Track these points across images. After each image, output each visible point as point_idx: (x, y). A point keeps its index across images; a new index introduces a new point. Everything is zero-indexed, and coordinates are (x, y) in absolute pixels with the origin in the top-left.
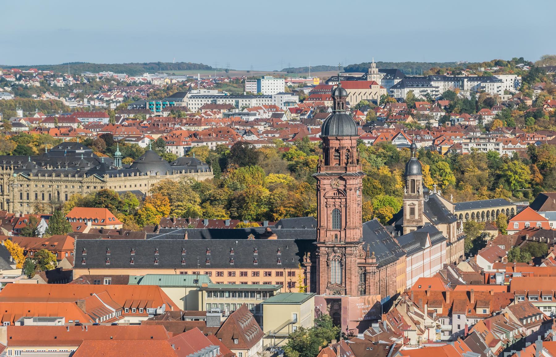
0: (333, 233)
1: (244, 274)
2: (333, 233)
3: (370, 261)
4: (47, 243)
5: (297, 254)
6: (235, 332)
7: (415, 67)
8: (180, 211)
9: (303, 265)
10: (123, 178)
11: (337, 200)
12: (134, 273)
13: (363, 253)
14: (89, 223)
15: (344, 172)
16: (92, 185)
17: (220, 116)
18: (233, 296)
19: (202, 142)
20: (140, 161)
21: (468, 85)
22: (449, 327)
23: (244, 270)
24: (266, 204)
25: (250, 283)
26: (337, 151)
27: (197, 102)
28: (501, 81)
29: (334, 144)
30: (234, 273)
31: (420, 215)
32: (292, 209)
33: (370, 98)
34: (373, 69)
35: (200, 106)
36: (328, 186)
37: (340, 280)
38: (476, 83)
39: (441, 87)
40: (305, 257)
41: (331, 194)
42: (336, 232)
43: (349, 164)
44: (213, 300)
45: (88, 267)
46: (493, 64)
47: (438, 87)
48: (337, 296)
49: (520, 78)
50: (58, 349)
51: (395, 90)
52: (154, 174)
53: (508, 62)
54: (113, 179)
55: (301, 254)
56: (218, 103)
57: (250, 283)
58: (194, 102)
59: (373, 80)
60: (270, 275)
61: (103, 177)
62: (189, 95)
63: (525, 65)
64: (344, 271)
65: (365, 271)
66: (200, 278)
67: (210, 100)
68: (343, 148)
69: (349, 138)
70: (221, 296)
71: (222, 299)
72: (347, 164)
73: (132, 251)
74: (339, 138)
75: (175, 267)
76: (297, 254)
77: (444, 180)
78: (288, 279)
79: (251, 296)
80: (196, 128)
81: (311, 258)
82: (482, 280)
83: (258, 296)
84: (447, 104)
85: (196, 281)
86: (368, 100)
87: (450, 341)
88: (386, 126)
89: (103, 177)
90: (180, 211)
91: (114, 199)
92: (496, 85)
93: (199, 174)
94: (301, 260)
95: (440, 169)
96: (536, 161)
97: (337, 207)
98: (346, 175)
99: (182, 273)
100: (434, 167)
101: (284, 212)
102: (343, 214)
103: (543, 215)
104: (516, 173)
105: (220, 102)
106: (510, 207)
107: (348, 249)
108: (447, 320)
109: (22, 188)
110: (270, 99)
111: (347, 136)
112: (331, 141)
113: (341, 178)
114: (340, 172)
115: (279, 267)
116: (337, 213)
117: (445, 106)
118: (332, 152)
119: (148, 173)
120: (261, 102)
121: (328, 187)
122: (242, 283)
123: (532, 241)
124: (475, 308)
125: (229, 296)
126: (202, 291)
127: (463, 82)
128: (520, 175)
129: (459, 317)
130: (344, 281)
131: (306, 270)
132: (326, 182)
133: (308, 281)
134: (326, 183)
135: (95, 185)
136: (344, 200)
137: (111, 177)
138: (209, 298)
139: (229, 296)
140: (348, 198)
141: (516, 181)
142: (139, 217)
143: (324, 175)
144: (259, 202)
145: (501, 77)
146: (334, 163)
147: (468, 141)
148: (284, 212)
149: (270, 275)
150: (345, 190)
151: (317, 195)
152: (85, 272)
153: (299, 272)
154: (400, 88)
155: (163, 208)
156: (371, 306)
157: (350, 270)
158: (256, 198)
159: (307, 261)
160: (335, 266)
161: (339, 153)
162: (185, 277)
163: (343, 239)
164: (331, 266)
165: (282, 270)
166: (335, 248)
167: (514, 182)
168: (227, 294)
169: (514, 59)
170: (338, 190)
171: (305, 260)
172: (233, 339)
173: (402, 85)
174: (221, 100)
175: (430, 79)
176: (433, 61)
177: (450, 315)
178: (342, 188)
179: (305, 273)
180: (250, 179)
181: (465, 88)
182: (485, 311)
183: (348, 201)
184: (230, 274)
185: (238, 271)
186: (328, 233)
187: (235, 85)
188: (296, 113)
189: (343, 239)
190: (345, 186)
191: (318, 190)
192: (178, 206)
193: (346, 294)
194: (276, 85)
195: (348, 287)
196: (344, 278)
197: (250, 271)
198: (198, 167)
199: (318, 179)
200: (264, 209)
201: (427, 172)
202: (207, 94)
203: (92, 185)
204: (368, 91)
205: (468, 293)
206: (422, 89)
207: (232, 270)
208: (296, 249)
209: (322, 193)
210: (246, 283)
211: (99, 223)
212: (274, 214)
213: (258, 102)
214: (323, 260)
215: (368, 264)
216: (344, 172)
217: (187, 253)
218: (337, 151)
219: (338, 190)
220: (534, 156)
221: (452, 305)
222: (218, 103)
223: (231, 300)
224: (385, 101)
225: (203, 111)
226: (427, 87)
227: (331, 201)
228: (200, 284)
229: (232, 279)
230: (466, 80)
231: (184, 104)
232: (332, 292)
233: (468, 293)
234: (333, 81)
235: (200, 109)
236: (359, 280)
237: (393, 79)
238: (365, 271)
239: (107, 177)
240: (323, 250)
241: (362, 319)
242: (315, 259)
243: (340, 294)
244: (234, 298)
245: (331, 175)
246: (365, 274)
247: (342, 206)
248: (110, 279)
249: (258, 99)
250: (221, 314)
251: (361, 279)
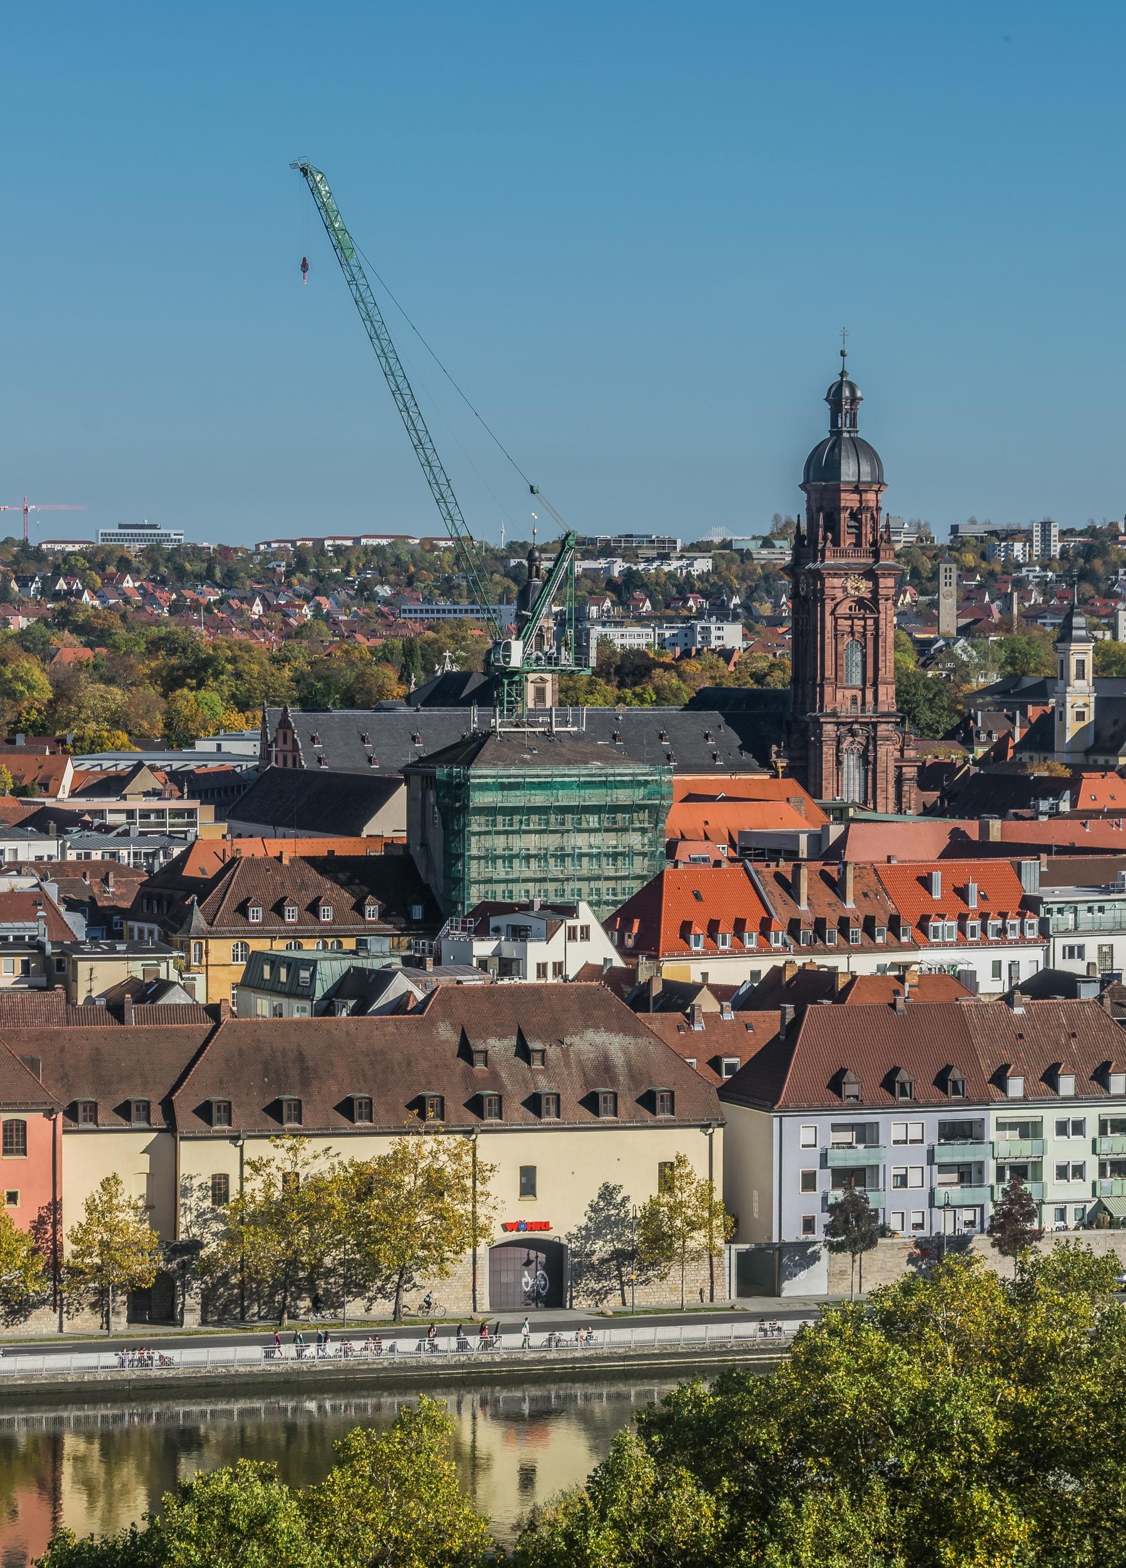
41: (843, 610)
42: (854, 692)
132: (837, 582)
136: (870, 622)
161: (860, 521)
183: (882, 623)
227: (844, 624)
240: (829, 730)
247: (869, 634)
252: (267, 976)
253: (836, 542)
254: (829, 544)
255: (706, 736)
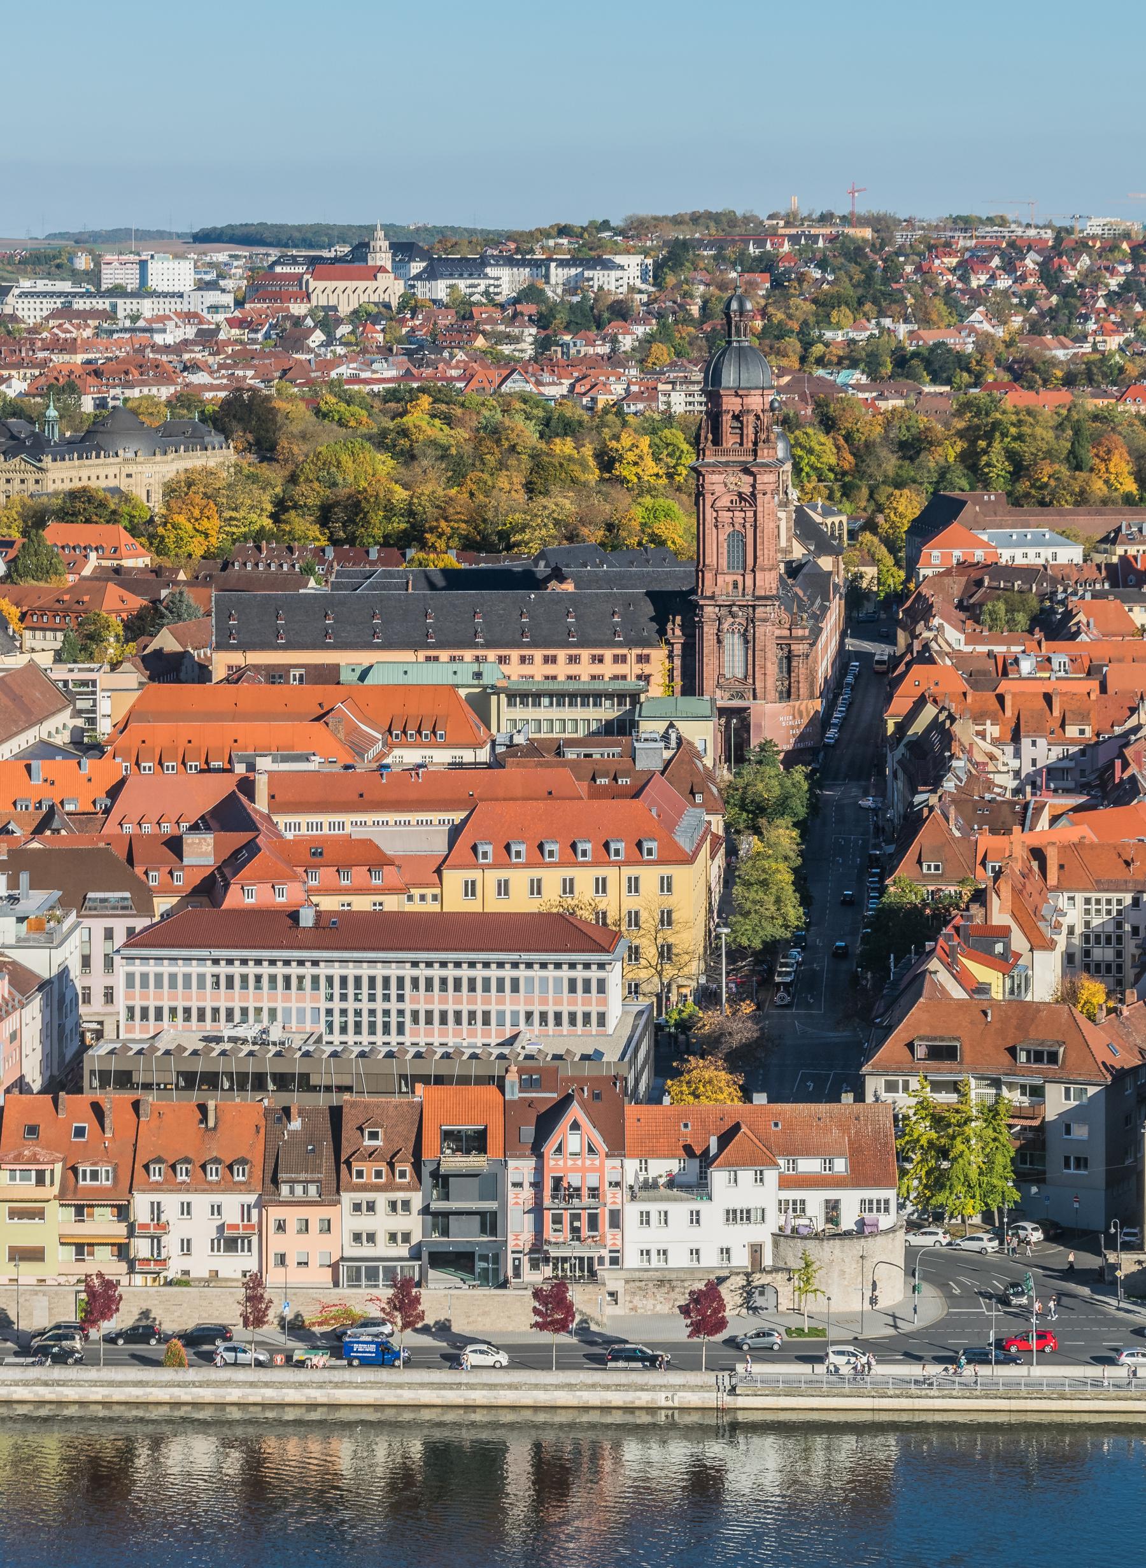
0: (730, 579)
1: (550, 660)
2: (730, 579)
3: (800, 633)
4: (66, 597)
5: (652, 619)
6: (695, 781)
7: (336, 233)
8: (234, 530)
9: (668, 642)
10: (77, 462)
11: (737, 514)
12: (348, 660)
13: (786, 617)
14: (93, 555)
15: (751, 459)
16: (17, 477)
17: (88, 333)
18: (558, 705)
19: (132, 387)
20: (101, 429)
21: (558, 275)
22: (1015, 764)
23: (550, 652)
24: (402, 515)
25: (561, 678)
26: (736, 417)
27: (32, 306)
28: (622, 268)
29: (731, 404)
30: (532, 658)
31: (789, 540)
32: (464, 526)
33: (375, 298)
34: (379, 243)
35: (45, 313)
36: (722, 485)
37: (743, 670)
38: (573, 271)
39: (507, 281)
40: (670, 626)
41: (724, 502)
42: (735, 577)
43: (761, 444)
44: (520, 712)
45: (244, 647)
46: (554, 232)
47: (498, 279)
48: (737, 703)
49: (649, 261)
50: (413, 817)
51: (419, 284)
52: (130, 455)
53: (584, 229)
54: (59, 464)
55: (661, 621)
56: (75, 306)
57: (585, 678)
58: (26, 306)
59: (379, 263)
60: (601, 661)
61: (40, 461)
62: (16, 291)
63: (616, 234)
64: (750, 652)
65: (790, 651)
66: (485, 668)
67: (58, 301)
68: (748, 411)
69: (760, 392)
70: (534, 705)
71: (537, 709)
72: (755, 444)
73: (326, 615)
74: (740, 392)
75: (415, 646)
76: (652, 619)
77: (677, 465)
78: (637, 669)
79: (595, 705)
80: (67, 357)
81: (683, 627)
82: (992, 668)
83: (608, 703)
84: (534, 312)
85: (478, 675)
86: (376, 304)
87: (489, 766)
88: (446, 354)
89: (40, 461)
90: (234, 530)
91: (102, 505)
92: (614, 274)
93: (209, 452)
94: (662, 632)
95: (668, 445)
96: (832, 427)
97: (737, 527)
98: (758, 465)
99: (428, 659)
100: (657, 441)
101: (448, 531)
102: (750, 541)
103: (985, 538)
104: (810, 451)
105: (80, 304)
106: (836, 520)
107: (759, 610)
108: (1009, 750)
109: (9, 487)
110: (179, 300)
111: (756, 388)
112: (725, 399)
113: (747, 471)
114: (742, 459)
115: (620, 645)
116: (737, 540)
117: (530, 316)
118: (727, 419)
119: (121, 452)
120: (167, 306)
121: (719, 489)
122: (547, 678)
123: (998, 588)
124: (1063, 726)
125: (551, 704)
126: (498, 694)
127: (548, 269)
128: (819, 457)
129: (1034, 743)
130: (750, 672)
131: (671, 651)
132: (715, 478)
133: (677, 673)
134: (714, 480)
135: (22, 476)
136: (750, 514)
137: (55, 460)
138: (512, 709)
139: (551, 704)
140: (760, 509)
141: (812, 467)
142: (161, 542)
143: (714, 465)
144: (390, 510)
145: (619, 259)
146: (730, 441)
147: (669, 387)
148: (448, 531)
149: (601, 661)
150: (753, 494)
151: (697, 504)
152: (237, 658)
153: (659, 655)
154: (428, 279)
155: (205, 524)
156: (805, 721)
157: (763, 650)
158: (384, 502)
159: (675, 632)
160: (734, 644)
161: (741, 422)
162: (455, 666)
163: (749, 591)
164: (725, 642)
165: (624, 651)
166: (735, 609)
167: (807, 469)
168: (545, 701)
169: (592, 223)
170: (740, 495)
171: (670, 632)
172: (692, 793)
173: (430, 274)
174: (81, 301)
175: (483, 262)
176: (440, 223)
177: (1016, 738)
178: (747, 490)
179: (670, 657)
180: (350, 464)
181: (553, 281)
182: (1082, 732)
183: (759, 515)
184: (523, 659)
185: (538, 654)
186: (720, 579)
187: (9, 268)
188: (240, 327)
189: (749, 591)
190: (754, 486)
191: (699, 494)
192: (232, 519)
193: (755, 698)
194: (177, 271)
195: (758, 685)
196: (750, 667)
197: (562, 654)
198: (207, 439)
199: (699, 473)
200: (400, 525)
201: (646, 449)
202: (50, 289)
203: (17, 477)
204: (371, 285)
205: (1048, 698)
206: (469, 282)
207: (526, 652)
208: (649, 609)
209: (709, 500)
210: (554, 678)
211: (107, 554)
212: (428, 536)
213: (156, 306)
214: (709, 631)
215: (797, 638)
216: (751, 459)
217: (437, 619)
218: (736, 417)
219: (740, 495)
220: (828, 418)
221: (1018, 718)
222: (75, 306)
223: (556, 713)
224: (410, 305)
225: (51, 323)
226: (479, 278)
227: (725, 516)
228: (486, 680)
229: (527, 670)
230: (553, 265)
231: (8, 310)
232: (727, 695)
233: (1048, 698)
234: (283, 264)
235: (47, 319)
236: (777, 670)
237: (409, 262)
238: (790, 651)
239: (47, 461)
240: (710, 611)
241: (789, 747)
242: (692, 631)
243: (742, 697)
244: (573, 709)
245: (726, 464)
246: (789, 659)
247: (748, 525)
248: (303, 671)
249: (156, 300)
250: (662, 744)
251: (781, 668)
252: (958, 993)
253: (717, 442)
254: (709, 444)
255: (614, 613)
